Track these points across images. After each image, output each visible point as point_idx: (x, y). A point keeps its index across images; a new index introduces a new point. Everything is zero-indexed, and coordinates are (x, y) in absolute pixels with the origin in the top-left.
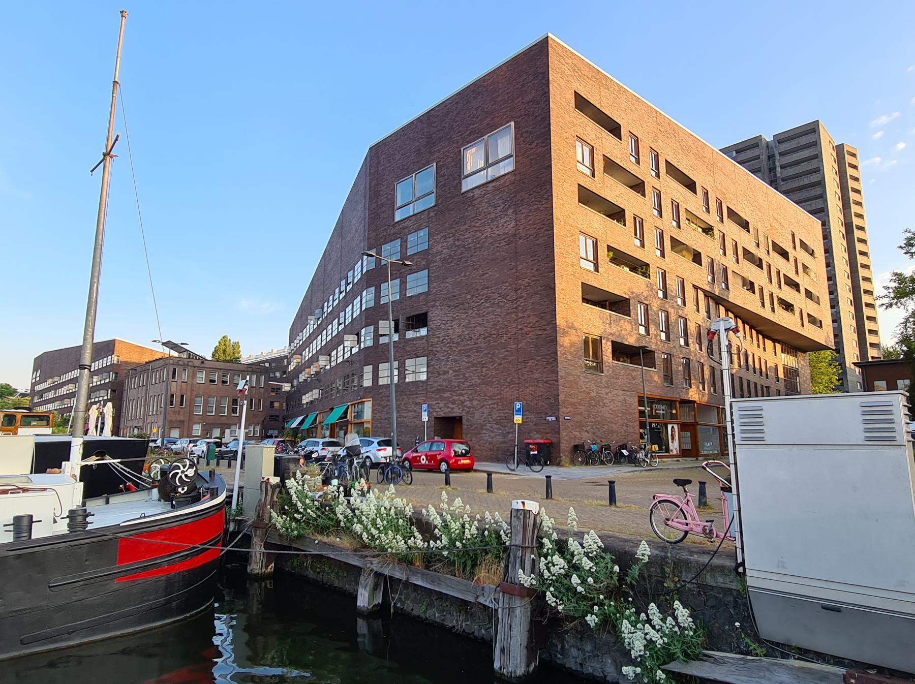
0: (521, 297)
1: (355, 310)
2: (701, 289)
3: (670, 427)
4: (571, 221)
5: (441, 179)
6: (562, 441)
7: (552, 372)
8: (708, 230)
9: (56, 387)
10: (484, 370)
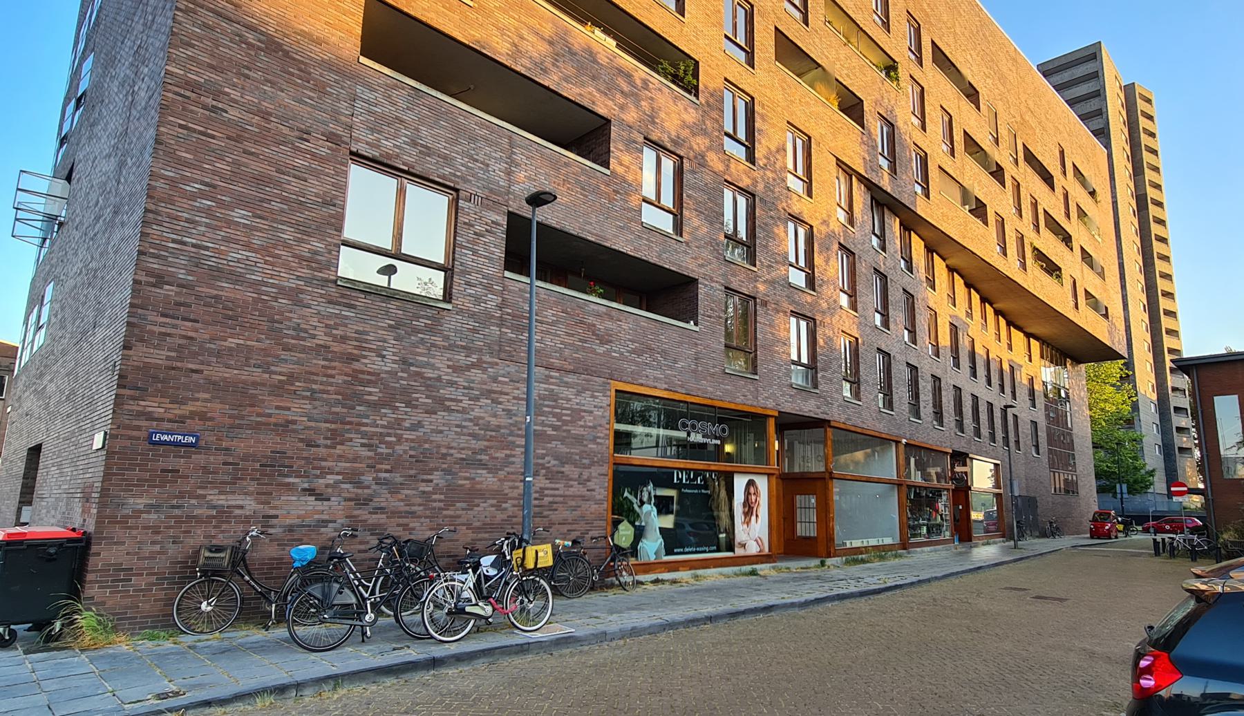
3: (740, 483)
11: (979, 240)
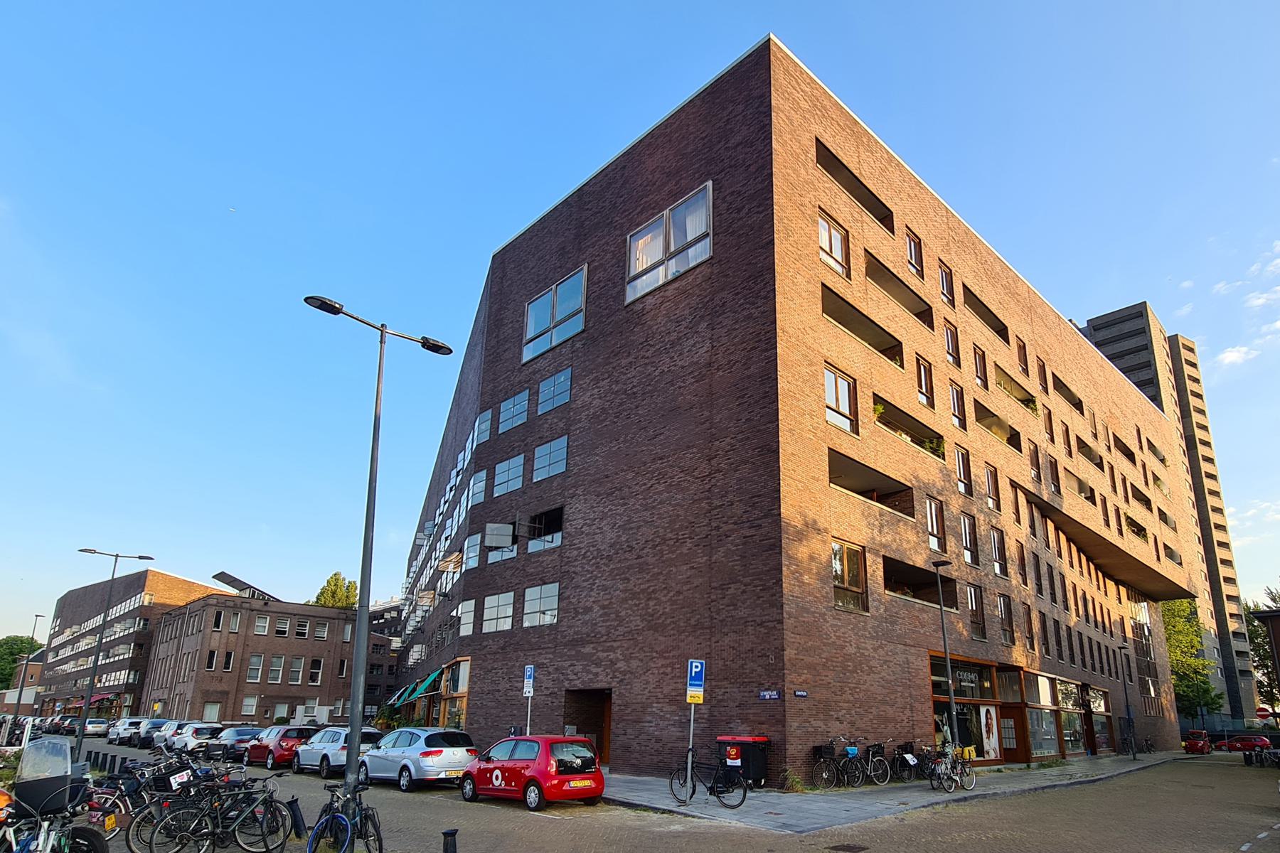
0: (719, 471)
1: (460, 515)
2: (1022, 488)
3: (983, 710)
4: (810, 342)
5: (595, 288)
6: (791, 739)
7: (772, 605)
8: (1029, 401)
9: (74, 641)
10: (651, 603)
11: (1089, 516)
